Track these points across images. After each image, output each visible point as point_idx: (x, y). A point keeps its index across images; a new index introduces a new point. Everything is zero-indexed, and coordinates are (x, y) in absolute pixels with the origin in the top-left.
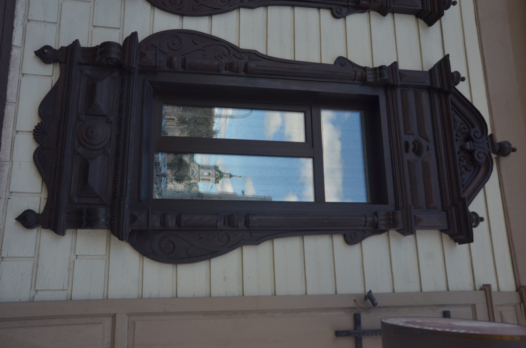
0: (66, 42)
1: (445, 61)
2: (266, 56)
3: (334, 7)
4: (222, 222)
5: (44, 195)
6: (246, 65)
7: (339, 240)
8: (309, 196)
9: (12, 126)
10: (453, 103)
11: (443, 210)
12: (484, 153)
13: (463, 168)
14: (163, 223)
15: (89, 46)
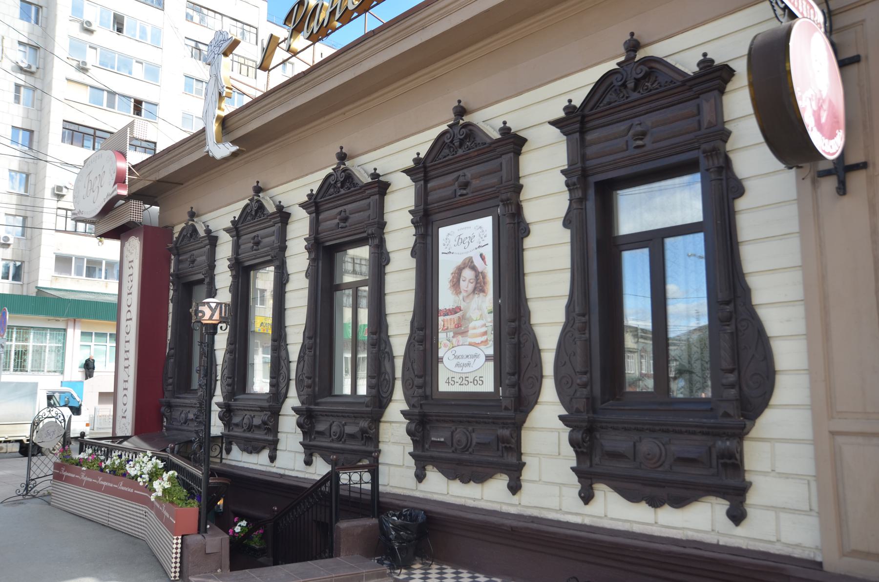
0: (574, 478)
1: (555, 123)
2: (569, 295)
3: (521, 236)
4: (728, 327)
5: (713, 499)
6: (579, 315)
7: (741, 204)
8: (699, 238)
9: (651, 527)
10: (592, 109)
11: (698, 97)
12: (637, 67)
13: (654, 86)
14: (732, 386)
15: (575, 458)
